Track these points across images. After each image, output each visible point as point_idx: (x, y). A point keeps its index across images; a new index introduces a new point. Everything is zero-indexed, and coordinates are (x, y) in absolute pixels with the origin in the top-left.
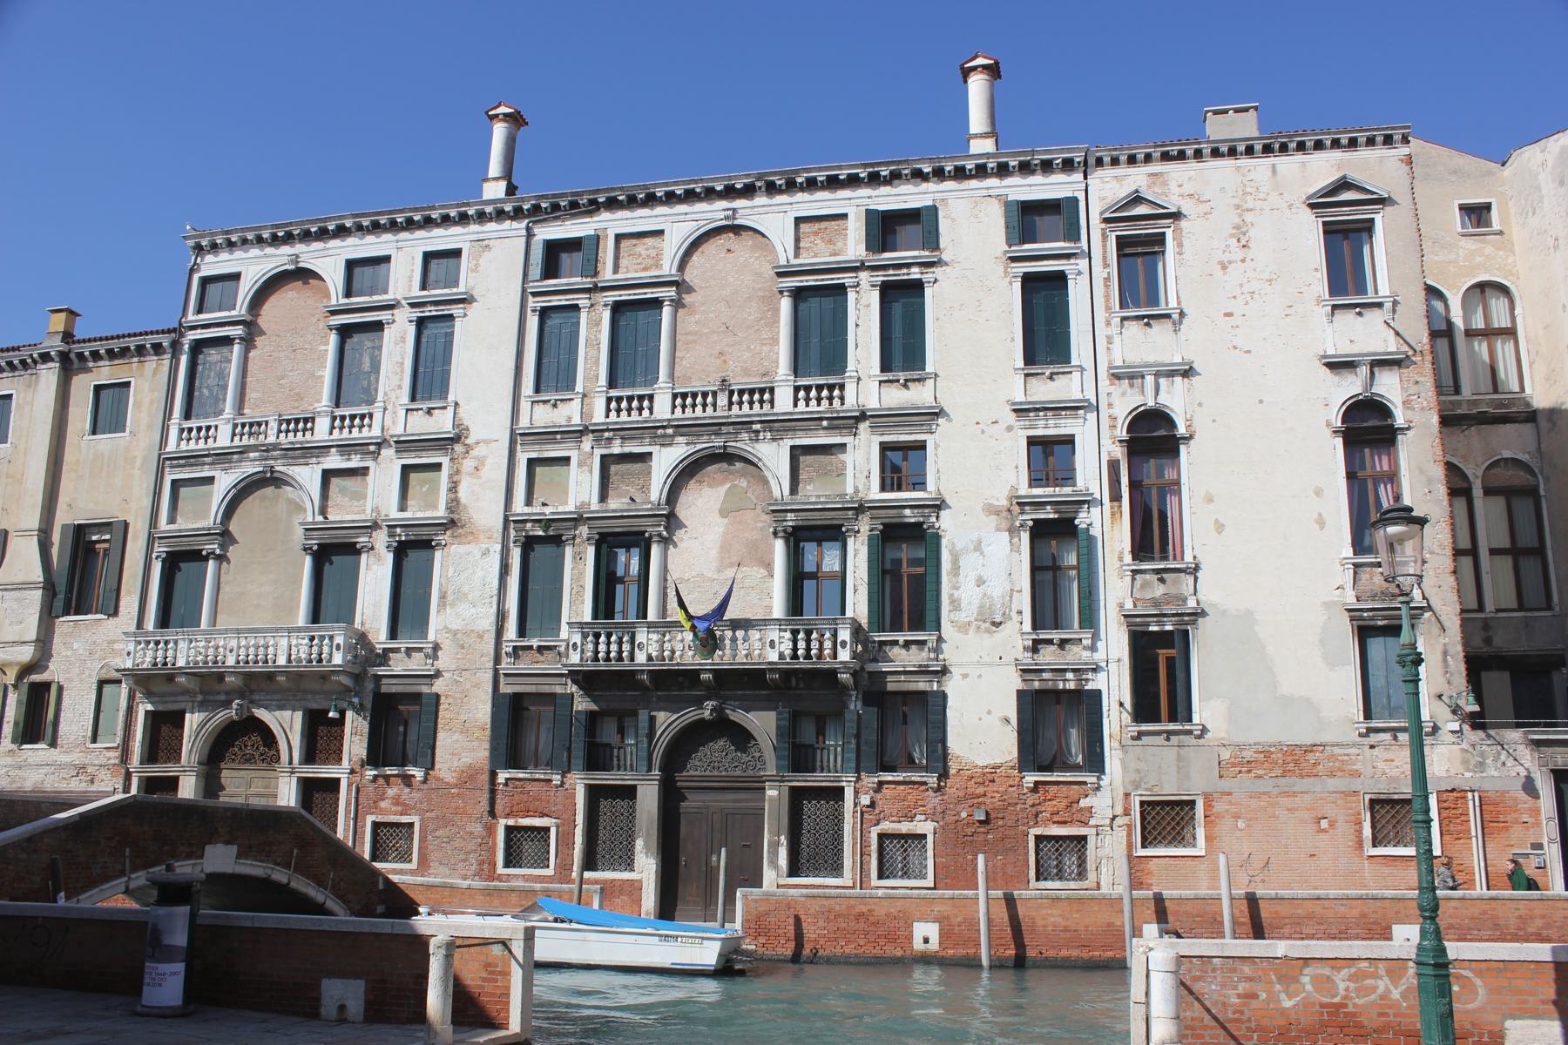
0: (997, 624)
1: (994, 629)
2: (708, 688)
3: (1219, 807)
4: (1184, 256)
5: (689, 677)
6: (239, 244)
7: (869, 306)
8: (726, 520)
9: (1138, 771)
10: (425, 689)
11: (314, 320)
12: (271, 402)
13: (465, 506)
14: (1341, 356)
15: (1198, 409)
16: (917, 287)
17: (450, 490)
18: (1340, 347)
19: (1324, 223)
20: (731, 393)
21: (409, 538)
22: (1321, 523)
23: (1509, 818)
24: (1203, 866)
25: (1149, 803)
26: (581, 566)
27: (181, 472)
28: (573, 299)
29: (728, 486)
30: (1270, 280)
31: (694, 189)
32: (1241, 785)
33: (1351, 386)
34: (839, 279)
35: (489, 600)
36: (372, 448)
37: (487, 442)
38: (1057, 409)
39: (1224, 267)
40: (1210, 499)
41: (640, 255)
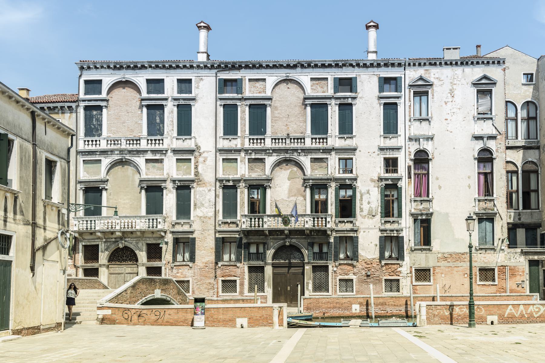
0: (374, 216)
1: (373, 217)
2: (286, 235)
3: (437, 271)
4: (434, 99)
5: (281, 232)
6: (100, 68)
7: (335, 111)
8: (290, 181)
9: (414, 260)
10: (191, 236)
11: (135, 101)
12: (120, 132)
13: (201, 174)
14: (479, 135)
15: (435, 150)
16: (351, 105)
17: (195, 168)
18: (478, 132)
19: (477, 90)
20: (291, 139)
21: (181, 185)
22: (469, 187)
23: (516, 274)
24: (432, 287)
25: (417, 270)
26: (243, 196)
27: (87, 157)
28: (235, 102)
29: (290, 170)
30: (459, 109)
31: (276, 65)
32: (443, 263)
33: (480, 145)
34: (325, 101)
35: (212, 206)
36: (164, 152)
37: (208, 152)
38: (393, 149)
39: (446, 104)
40: (437, 179)
41: (258, 87)
